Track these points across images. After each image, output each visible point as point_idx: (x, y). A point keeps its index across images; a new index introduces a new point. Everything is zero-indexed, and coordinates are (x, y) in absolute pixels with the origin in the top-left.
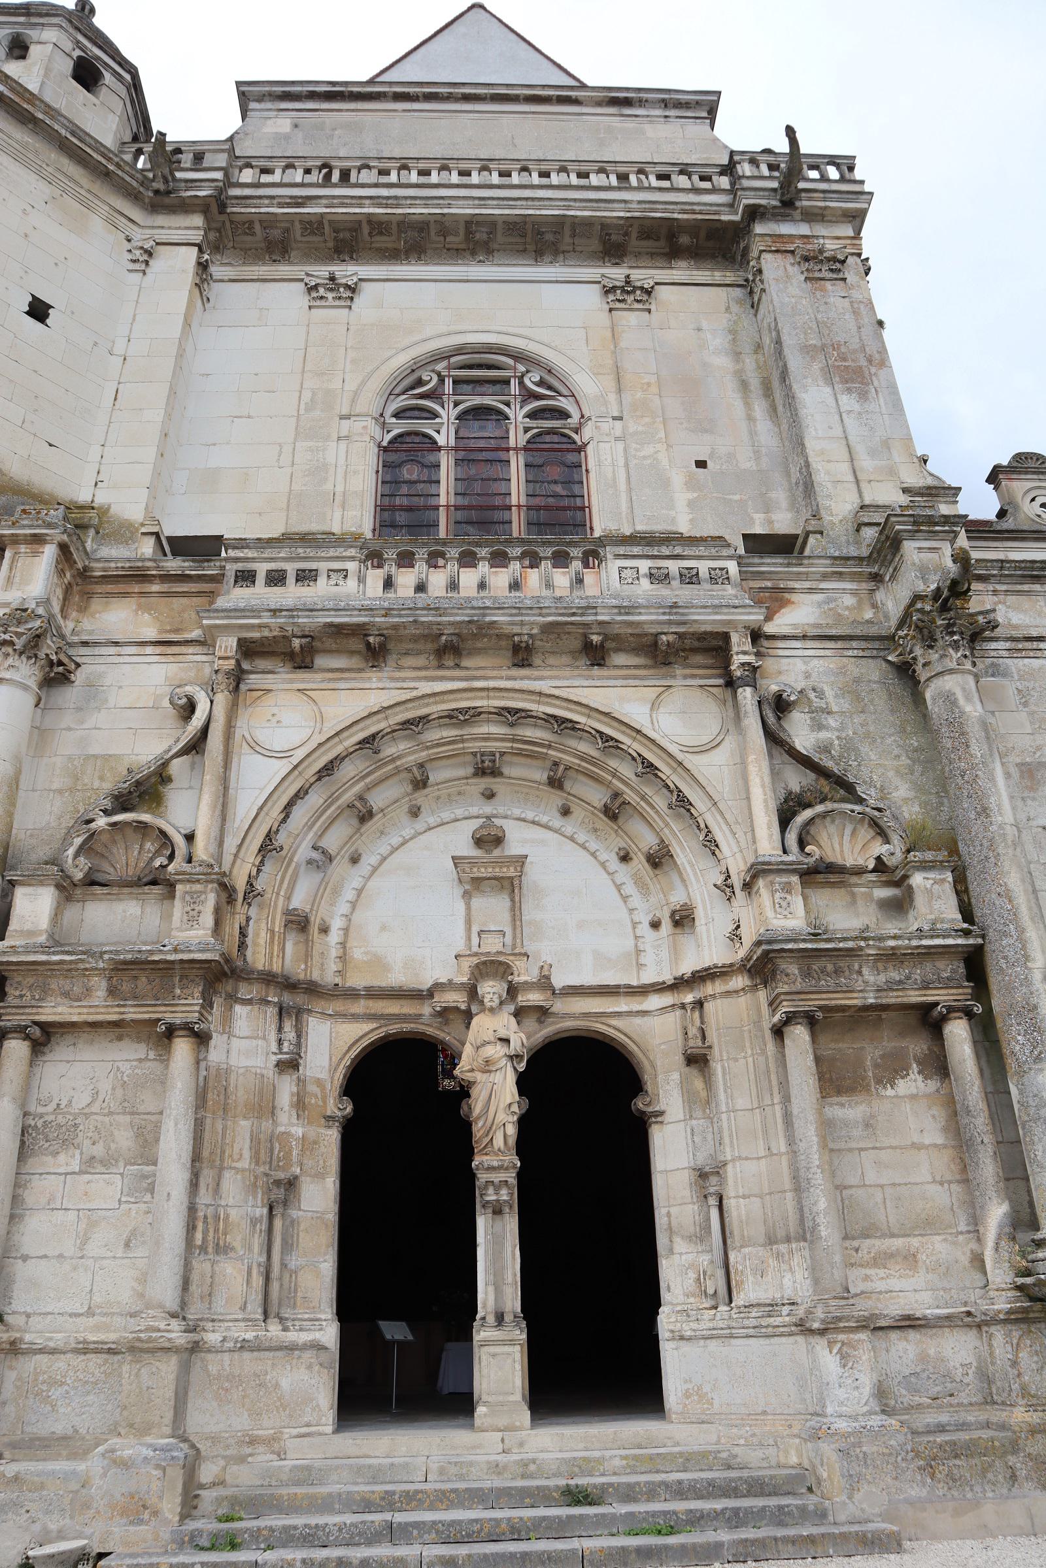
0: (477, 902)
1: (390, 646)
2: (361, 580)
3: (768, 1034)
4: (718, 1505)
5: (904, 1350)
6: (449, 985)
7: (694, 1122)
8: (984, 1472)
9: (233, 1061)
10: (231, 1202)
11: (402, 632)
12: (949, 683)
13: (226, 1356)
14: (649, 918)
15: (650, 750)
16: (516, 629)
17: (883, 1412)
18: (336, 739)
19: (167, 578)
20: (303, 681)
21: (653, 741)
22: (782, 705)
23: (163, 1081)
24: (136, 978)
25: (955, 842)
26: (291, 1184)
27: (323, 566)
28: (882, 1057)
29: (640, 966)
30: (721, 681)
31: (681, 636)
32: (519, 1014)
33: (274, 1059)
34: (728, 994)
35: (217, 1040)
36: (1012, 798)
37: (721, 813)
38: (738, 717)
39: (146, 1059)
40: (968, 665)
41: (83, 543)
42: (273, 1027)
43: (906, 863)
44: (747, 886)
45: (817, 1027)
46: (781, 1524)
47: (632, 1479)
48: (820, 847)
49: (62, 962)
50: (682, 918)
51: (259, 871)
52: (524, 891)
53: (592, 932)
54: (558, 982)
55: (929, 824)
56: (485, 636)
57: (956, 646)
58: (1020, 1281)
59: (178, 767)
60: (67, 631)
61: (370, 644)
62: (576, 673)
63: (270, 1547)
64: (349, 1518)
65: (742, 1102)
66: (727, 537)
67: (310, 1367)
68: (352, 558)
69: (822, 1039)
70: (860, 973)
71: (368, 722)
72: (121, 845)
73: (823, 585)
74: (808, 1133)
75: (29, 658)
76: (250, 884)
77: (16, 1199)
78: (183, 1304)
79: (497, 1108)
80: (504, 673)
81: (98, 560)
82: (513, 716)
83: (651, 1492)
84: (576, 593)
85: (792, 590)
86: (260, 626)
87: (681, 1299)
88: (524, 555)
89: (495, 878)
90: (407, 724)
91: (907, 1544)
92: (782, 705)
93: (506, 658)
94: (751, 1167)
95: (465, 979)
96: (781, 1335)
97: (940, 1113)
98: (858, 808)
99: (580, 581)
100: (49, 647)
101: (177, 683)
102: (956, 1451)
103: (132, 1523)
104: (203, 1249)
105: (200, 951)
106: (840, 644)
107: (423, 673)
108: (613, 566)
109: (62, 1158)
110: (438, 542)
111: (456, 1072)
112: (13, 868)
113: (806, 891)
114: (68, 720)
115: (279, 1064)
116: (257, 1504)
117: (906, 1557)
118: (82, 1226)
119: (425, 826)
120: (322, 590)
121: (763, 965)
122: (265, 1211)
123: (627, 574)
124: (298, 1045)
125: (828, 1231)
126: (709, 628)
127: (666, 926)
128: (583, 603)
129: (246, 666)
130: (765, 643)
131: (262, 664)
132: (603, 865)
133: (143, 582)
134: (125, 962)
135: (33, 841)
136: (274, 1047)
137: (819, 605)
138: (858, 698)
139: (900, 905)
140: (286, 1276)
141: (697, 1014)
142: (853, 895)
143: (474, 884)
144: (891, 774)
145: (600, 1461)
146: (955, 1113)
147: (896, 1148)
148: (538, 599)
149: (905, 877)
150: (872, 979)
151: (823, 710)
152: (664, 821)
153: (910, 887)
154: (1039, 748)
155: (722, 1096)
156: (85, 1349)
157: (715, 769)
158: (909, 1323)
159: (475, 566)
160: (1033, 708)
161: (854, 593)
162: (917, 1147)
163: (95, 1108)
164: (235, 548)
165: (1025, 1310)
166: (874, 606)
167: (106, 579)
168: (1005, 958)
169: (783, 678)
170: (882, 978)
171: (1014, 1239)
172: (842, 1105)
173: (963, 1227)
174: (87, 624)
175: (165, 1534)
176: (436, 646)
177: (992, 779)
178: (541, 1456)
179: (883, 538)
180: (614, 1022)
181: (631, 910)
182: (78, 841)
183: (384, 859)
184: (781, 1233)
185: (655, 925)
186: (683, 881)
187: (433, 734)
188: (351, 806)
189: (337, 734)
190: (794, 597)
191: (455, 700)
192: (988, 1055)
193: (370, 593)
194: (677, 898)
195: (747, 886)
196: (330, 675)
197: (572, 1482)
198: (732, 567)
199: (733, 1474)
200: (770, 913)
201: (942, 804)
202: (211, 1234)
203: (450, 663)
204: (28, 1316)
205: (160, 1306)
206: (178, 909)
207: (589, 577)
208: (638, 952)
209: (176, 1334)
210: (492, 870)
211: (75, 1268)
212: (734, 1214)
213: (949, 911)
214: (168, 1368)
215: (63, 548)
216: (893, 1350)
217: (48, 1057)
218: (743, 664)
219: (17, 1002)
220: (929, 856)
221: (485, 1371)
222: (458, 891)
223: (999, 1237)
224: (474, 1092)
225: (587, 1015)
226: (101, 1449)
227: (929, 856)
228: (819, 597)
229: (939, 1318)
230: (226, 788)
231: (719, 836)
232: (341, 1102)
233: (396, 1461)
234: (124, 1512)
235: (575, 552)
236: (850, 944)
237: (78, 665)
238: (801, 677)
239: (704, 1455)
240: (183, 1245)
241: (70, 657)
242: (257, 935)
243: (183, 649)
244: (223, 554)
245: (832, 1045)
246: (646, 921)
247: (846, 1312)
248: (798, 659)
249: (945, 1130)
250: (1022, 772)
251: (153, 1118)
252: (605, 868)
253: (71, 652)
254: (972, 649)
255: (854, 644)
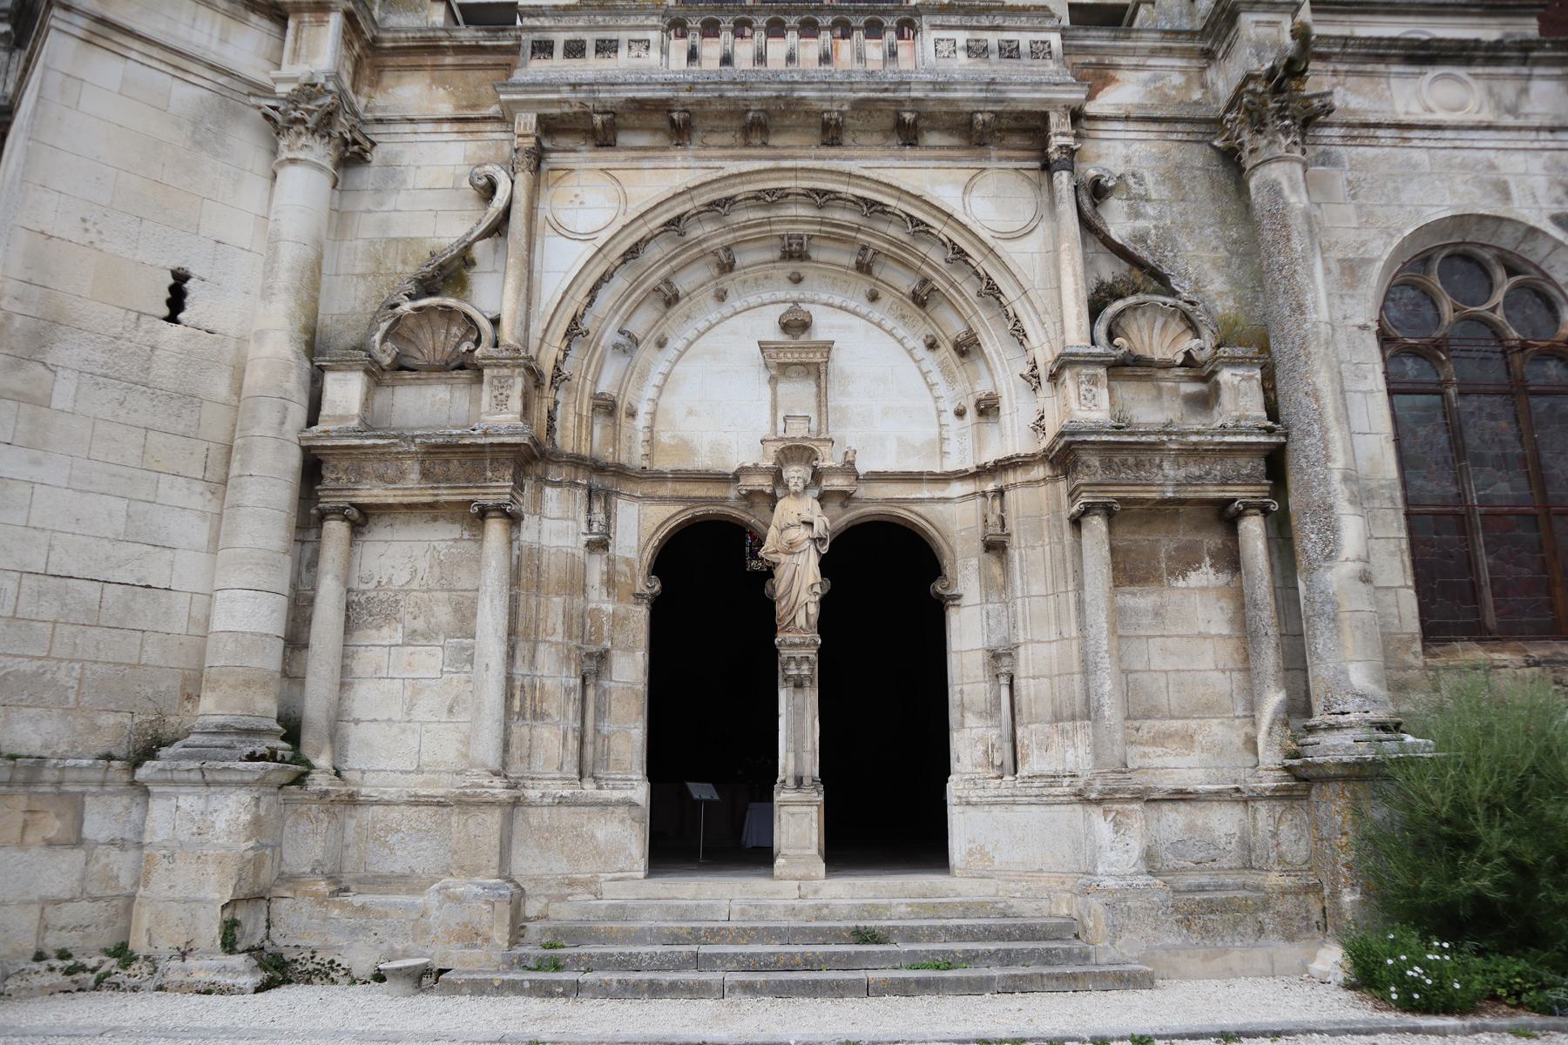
0: (784, 387)
1: (696, 122)
2: (664, 51)
3: (1066, 523)
4: (993, 946)
5: (1174, 820)
6: (755, 469)
7: (990, 606)
8: (1236, 924)
9: (545, 541)
10: (546, 672)
11: (707, 108)
12: (1276, 172)
13: (546, 810)
14: (954, 406)
15: (962, 235)
16: (826, 106)
17: (1149, 873)
18: (641, 221)
19: (460, 49)
20: (606, 160)
21: (964, 226)
22: (1098, 191)
23: (478, 561)
24: (448, 461)
25: (1267, 340)
26: (603, 657)
27: (623, 36)
28: (1176, 549)
29: (943, 454)
30: (1037, 164)
31: (997, 115)
32: (823, 498)
33: (584, 539)
34: (1029, 483)
35: (529, 521)
36: (1329, 295)
37: (1031, 303)
38: (1053, 204)
39: (461, 539)
40: (1297, 153)
41: (370, 11)
42: (584, 508)
43: (1214, 359)
44: (1054, 377)
45: (1115, 518)
46: (1048, 963)
47: (916, 923)
48: (1129, 339)
49: (375, 446)
50: (987, 407)
51: (565, 355)
52: (831, 377)
53: (895, 416)
54: (863, 467)
55: (1242, 319)
56: (793, 112)
57: (1286, 131)
58: (1288, 762)
59: (481, 250)
60: (360, 108)
61: (673, 121)
62: (887, 153)
63: (589, 970)
64: (659, 949)
65: (1037, 588)
66: (1051, 7)
67: (623, 821)
68: (654, 28)
69: (1119, 530)
70: (1160, 467)
71: (673, 203)
72: (427, 330)
73: (1151, 62)
74: (1099, 620)
75: (322, 137)
76: (557, 368)
77: (345, 670)
78: (504, 764)
79: (799, 584)
80: (813, 152)
81: (387, 30)
82: (822, 198)
83: (933, 934)
84: (890, 67)
85: (1117, 67)
86: (559, 102)
87: (970, 768)
88: (835, 24)
89: (801, 364)
90: (713, 205)
91: (1159, 982)
92: (1098, 191)
93: (814, 137)
94: (1043, 650)
95: (770, 464)
96: (1061, 803)
97: (1227, 605)
98: (1170, 301)
99: (893, 53)
100: (342, 125)
101: (476, 162)
102: (1212, 907)
103: (467, 947)
104: (521, 715)
105: (509, 435)
106: (1164, 127)
107: (729, 152)
108: (929, 37)
109: (385, 631)
110: (745, 10)
111: (761, 553)
112: (321, 353)
113: (1113, 383)
114: (366, 202)
115: (589, 544)
116: (577, 935)
117: (1156, 992)
118: (408, 693)
119: (731, 310)
120: (622, 63)
121: (1065, 456)
122: (579, 681)
123: (943, 46)
124: (608, 526)
125: (1111, 711)
126: (1027, 107)
127: (971, 414)
128: (896, 78)
129: (546, 144)
130: (1086, 124)
131: (564, 142)
132: (910, 352)
133: (436, 53)
134: (436, 446)
135: (340, 327)
136: (584, 528)
137: (1145, 83)
138: (1178, 185)
139: (1206, 401)
140: (599, 741)
141: (997, 502)
142: (1160, 389)
143: (780, 370)
144: (1207, 266)
145: (888, 907)
146: (1243, 606)
147: (1182, 636)
148: (849, 73)
149: (1214, 373)
150: (1172, 473)
151: (1141, 198)
152: (973, 309)
153: (1217, 383)
154: (1363, 244)
155: (1018, 582)
156: (416, 802)
157: (1026, 256)
158: (1181, 797)
159: (783, 36)
160: (1361, 200)
161: (1184, 71)
162: (1203, 636)
163: (415, 585)
164: (530, 16)
165: (1290, 789)
166: (1203, 86)
167: (398, 51)
168: (1306, 457)
169: (1102, 162)
170: (1182, 473)
171: (1287, 725)
172: (1134, 594)
173: (1240, 712)
174: (380, 100)
175: (497, 957)
176: (742, 123)
177: (1311, 276)
178: (834, 902)
179: (1219, 9)
180: (916, 508)
181: (937, 399)
182: (384, 326)
183: (691, 343)
184: (1066, 712)
185: (960, 414)
186: (990, 370)
187: (741, 216)
188: (656, 290)
189: (641, 216)
190: (1120, 75)
191: (763, 181)
192: (1280, 551)
193: (674, 65)
194: (983, 387)
195: (1054, 377)
196: (633, 154)
197: (861, 924)
198: (1055, 40)
199: (1008, 922)
200: (1074, 405)
201: (1257, 299)
202: (528, 702)
203: (757, 141)
204: (363, 772)
205: (484, 765)
206: (486, 393)
207: (903, 49)
208: (942, 440)
209: (499, 790)
210: (798, 356)
211: (404, 731)
212: (1024, 693)
213: (1254, 407)
214: (493, 819)
215: (349, 16)
216: (1164, 820)
217: (368, 537)
218: (1061, 147)
219: (333, 485)
220: (1239, 352)
221: (784, 828)
222: (765, 376)
223: (1273, 723)
224: (778, 573)
225: (889, 501)
226: (436, 886)
227: (1239, 352)
228: (1145, 75)
229: (1209, 793)
230: (530, 272)
231: (1027, 325)
232: (650, 580)
233: (702, 903)
234: (459, 938)
235: (890, 22)
236: (1152, 438)
237: (373, 144)
238: (1120, 162)
239: (983, 905)
240: (502, 711)
241: (364, 136)
242: (565, 419)
243: (482, 127)
244: (519, 23)
245: (1128, 537)
246: (951, 410)
247: (1123, 784)
248: (1118, 143)
249: (1232, 621)
250: (1343, 268)
251: (470, 594)
252: (911, 355)
253: (366, 130)
254: (1303, 135)
255: (1179, 127)
